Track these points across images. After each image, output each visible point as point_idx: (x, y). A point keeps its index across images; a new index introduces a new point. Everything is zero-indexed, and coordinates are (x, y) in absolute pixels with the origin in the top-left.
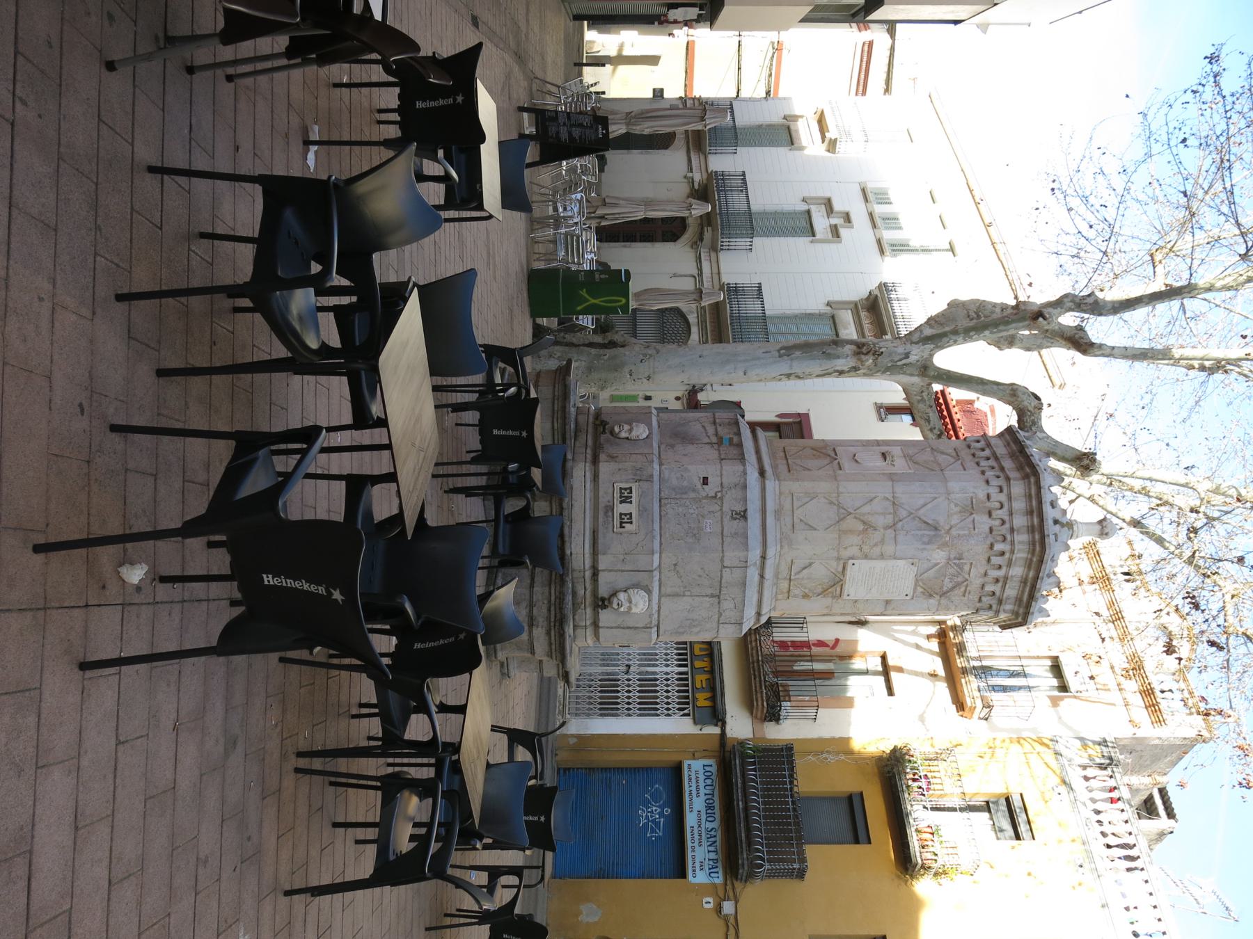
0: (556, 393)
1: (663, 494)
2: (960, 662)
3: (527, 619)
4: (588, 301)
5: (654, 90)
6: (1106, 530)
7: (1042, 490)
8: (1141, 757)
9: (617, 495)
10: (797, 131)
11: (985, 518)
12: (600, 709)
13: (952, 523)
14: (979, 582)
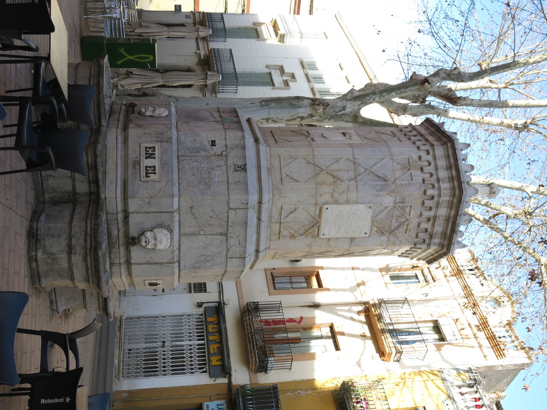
0: (92, 73)
1: (180, 153)
2: (380, 326)
3: (66, 249)
4: (127, 57)
5: (175, 6)
6: (494, 190)
7: (457, 151)
8: (490, 380)
9: (143, 152)
10: (261, 31)
11: (419, 172)
12: (145, 372)
13: (397, 176)
14: (416, 221)
